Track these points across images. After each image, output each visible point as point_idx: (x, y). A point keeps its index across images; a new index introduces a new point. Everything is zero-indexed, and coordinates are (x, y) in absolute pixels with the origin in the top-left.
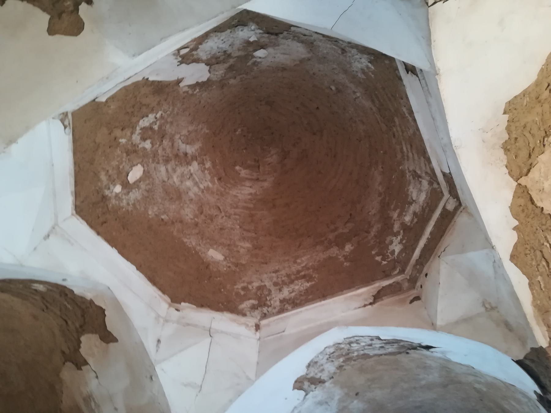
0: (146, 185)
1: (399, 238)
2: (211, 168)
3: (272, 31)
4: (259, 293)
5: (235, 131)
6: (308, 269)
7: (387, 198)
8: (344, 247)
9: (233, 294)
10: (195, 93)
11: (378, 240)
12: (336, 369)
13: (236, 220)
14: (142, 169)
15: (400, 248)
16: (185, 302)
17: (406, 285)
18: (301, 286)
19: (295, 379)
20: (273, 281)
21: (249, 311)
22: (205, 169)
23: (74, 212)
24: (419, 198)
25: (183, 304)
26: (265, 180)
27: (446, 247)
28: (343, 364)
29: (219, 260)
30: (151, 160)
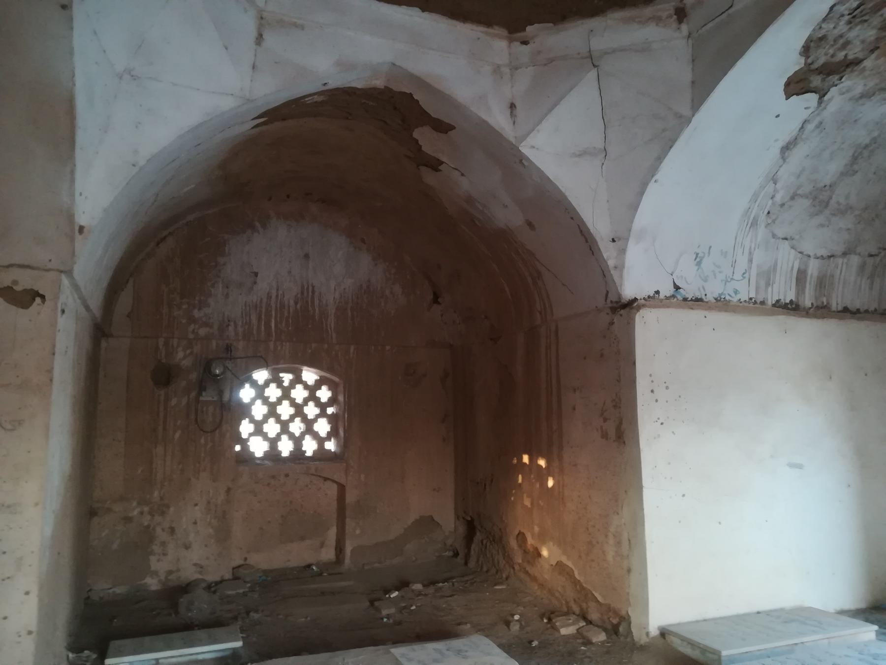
25: (529, 29)
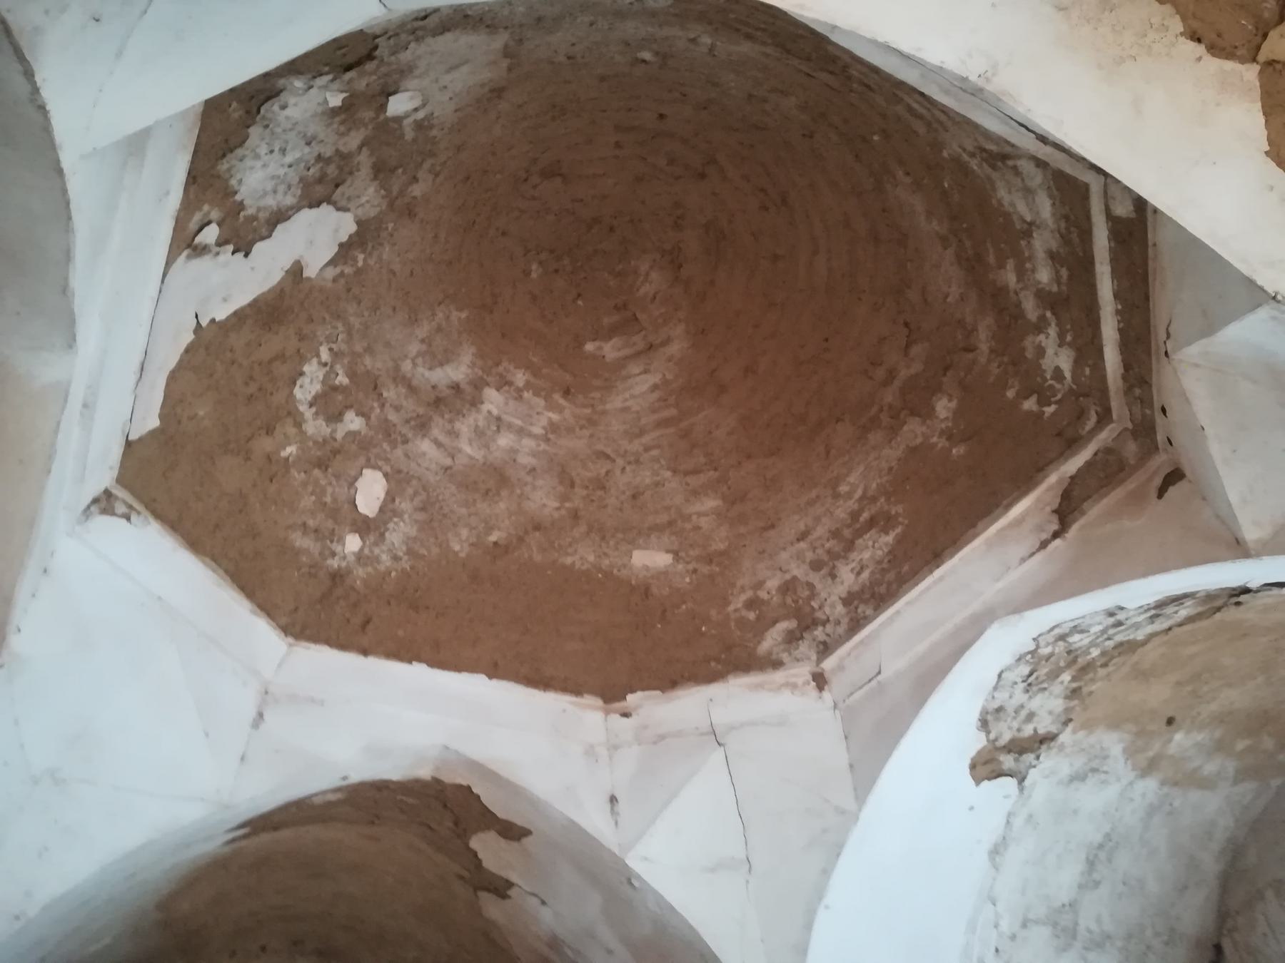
0: (412, 500)
1: (1053, 331)
2: (532, 380)
3: (350, 59)
4: (789, 601)
5: (527, 273)
6: (874, 499)
7: (968, 244)
8: (933, 409)
9: (733, 628)
10: (360, 264)
11: (1006, 359)
12: (1067, 701)
13: (656, 460)
14: (379, 475)
15: (1068, 357)
16: (633, 691)
17: (1131, 449)
18: (875, 547)
19: (968, 762)
20: (808, 560)
21: (784, 651)
22: (519, 390)
23: (290, 640)
24: (1038, 213)
25: (630, 697)
26: (667, 342)
27: (1168, 326)
28: (1075, 685)
29: (666, 566)
30: (385, 446)
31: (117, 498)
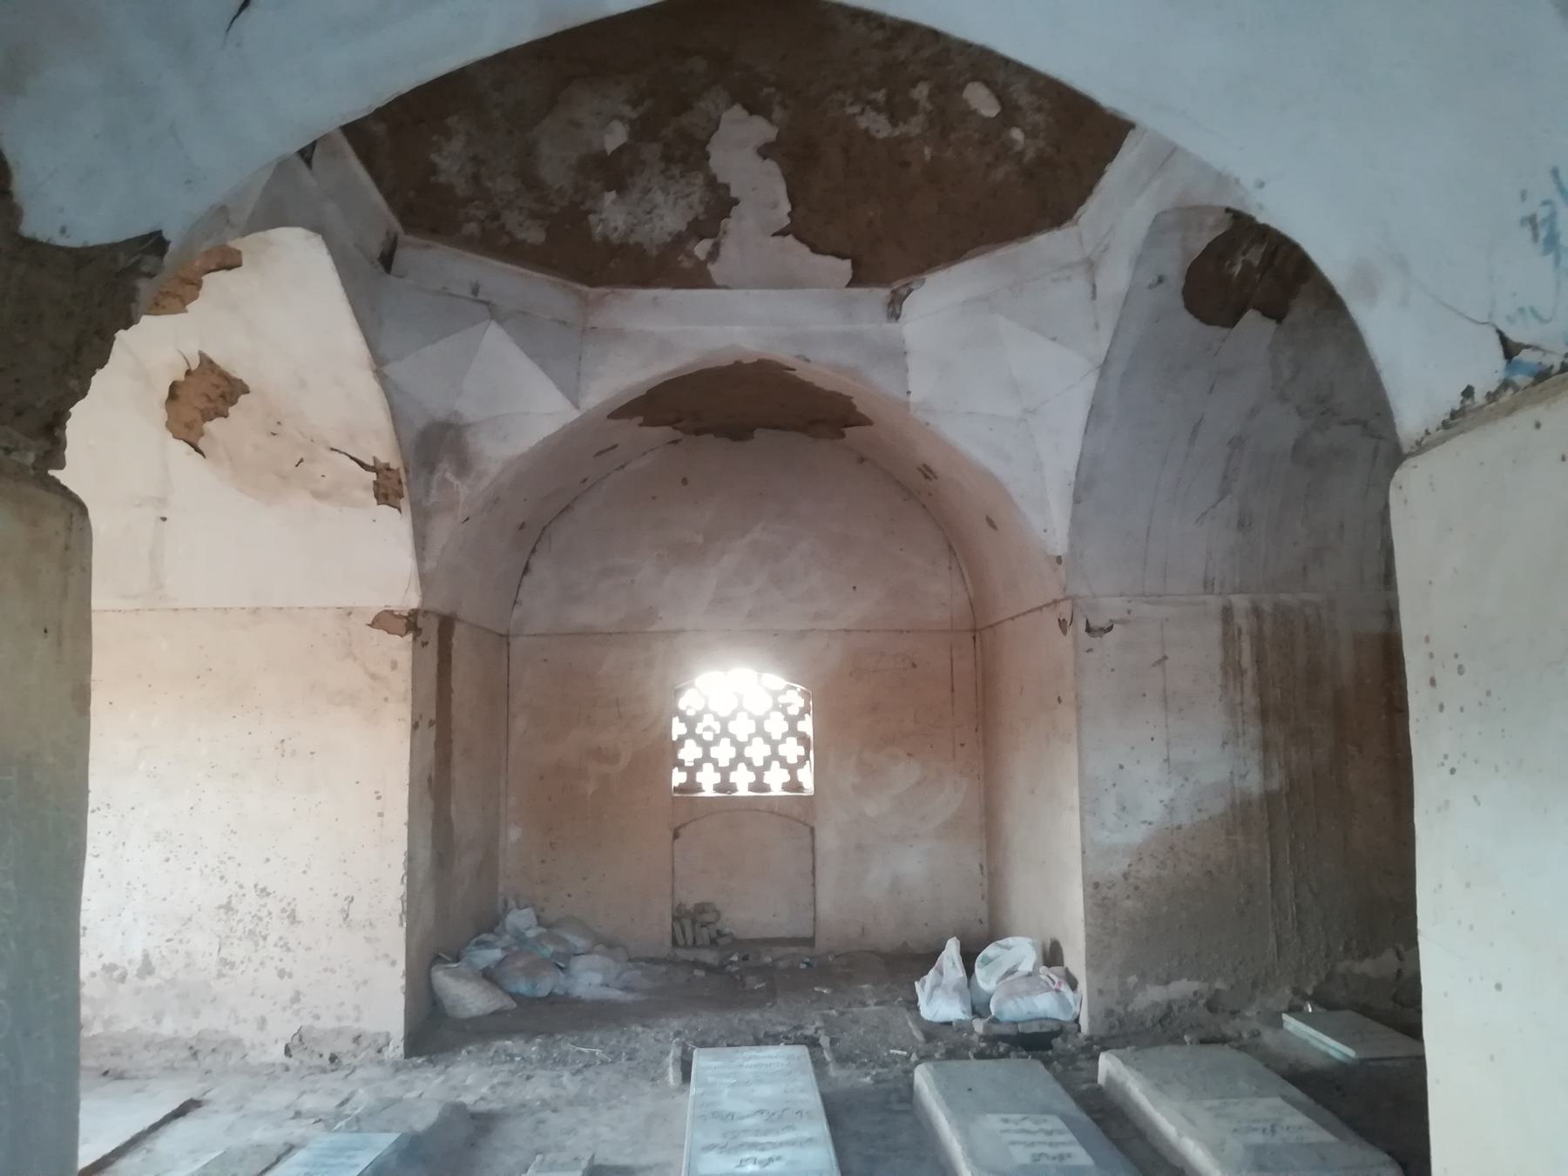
30: (950, 67)
31: (897, 289)
